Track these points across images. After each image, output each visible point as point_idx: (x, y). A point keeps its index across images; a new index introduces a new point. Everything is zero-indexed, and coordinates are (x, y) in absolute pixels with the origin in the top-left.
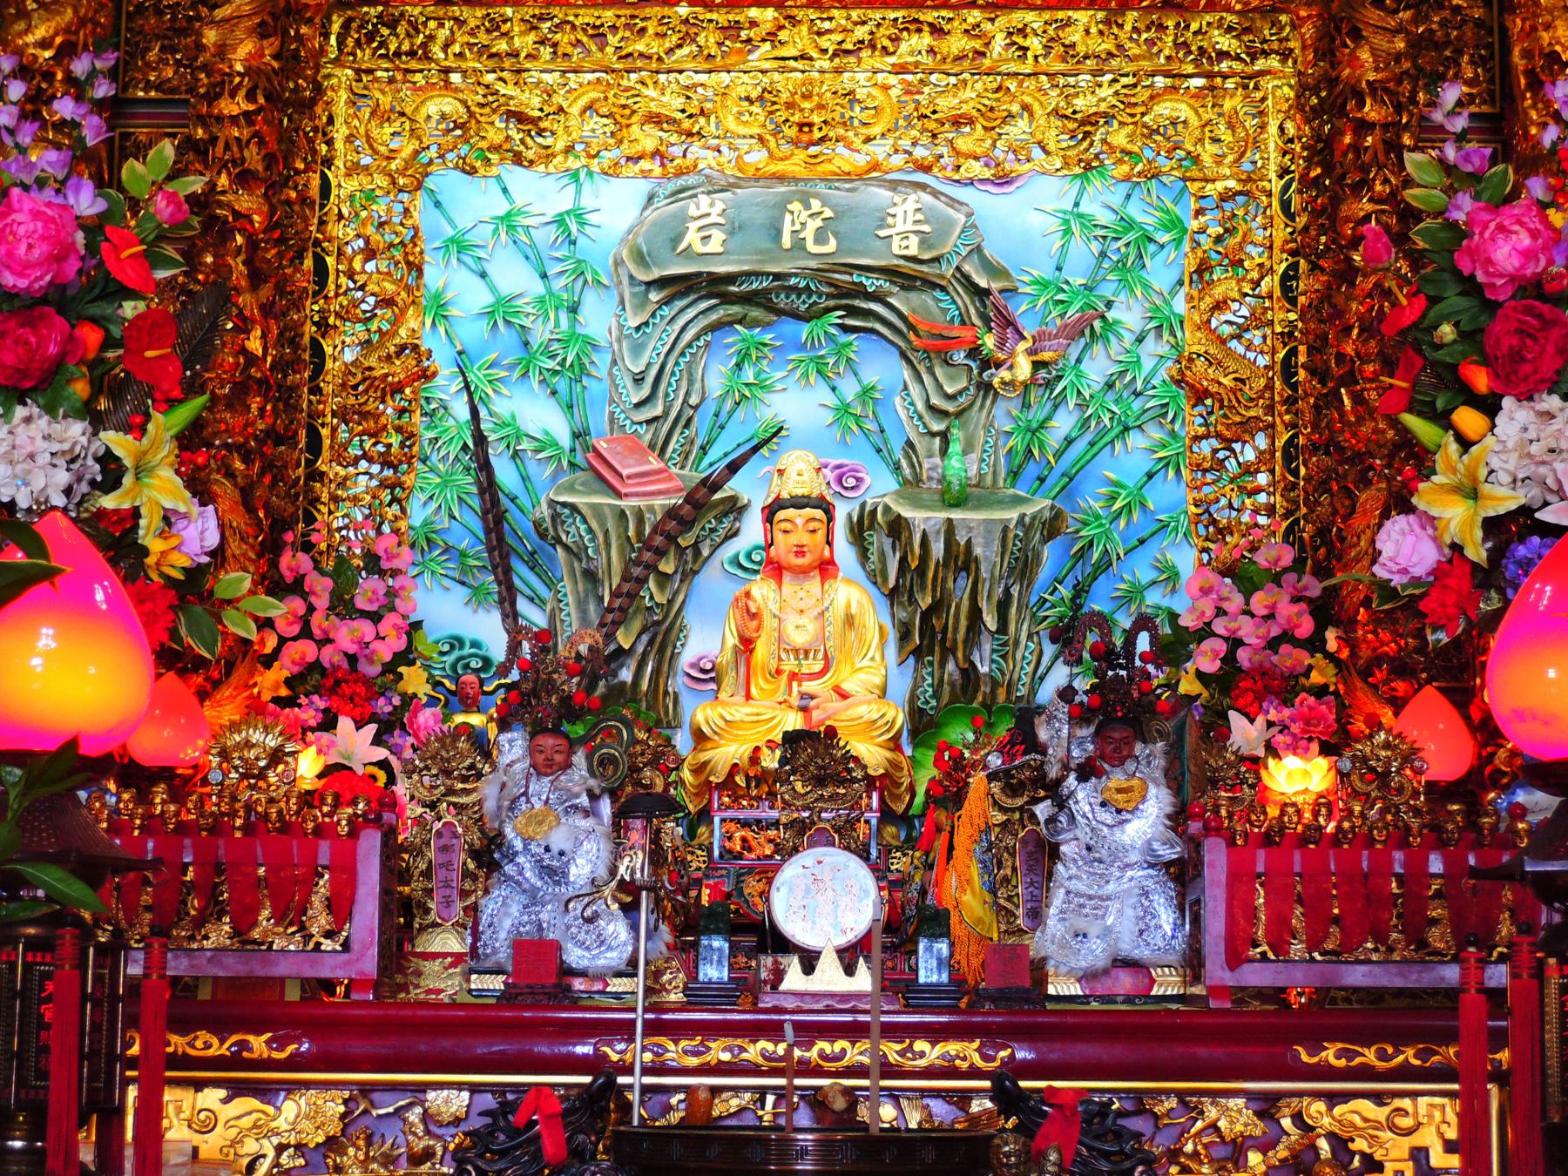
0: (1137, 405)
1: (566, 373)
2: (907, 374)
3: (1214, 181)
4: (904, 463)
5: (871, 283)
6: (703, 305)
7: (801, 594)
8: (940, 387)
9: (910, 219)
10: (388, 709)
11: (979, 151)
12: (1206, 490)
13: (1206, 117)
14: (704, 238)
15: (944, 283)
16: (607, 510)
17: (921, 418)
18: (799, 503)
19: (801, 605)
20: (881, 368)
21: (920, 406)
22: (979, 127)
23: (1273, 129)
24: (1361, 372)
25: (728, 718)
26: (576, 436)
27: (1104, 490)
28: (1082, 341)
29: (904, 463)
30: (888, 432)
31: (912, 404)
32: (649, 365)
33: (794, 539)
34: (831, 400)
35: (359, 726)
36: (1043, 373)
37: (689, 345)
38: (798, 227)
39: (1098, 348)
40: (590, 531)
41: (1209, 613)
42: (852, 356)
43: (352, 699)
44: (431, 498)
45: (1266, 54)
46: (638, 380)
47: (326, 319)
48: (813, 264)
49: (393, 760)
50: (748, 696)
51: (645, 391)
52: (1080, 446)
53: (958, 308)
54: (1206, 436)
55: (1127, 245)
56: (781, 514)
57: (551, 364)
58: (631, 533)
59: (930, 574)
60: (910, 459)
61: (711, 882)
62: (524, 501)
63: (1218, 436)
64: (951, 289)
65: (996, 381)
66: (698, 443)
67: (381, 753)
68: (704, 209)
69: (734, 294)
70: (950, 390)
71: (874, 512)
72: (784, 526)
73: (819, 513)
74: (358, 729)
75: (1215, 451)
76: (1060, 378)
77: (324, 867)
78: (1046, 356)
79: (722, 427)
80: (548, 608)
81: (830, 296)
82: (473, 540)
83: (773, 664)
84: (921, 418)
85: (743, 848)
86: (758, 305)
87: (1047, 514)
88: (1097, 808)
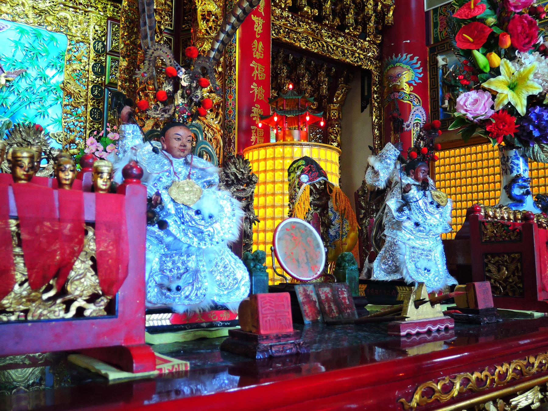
0: (34, 96)
3: (75, 37)
11: (8, 12)
12: (68, 119)
13: (74, 19)
22: (8, 5)
23: (91, 27)
24: (148, 88)
27: (23, 118)
28: (19, 77)
36: (8, 83)
39: (23, 80)
41: (94, 150)
45: (92, 7)
52: (16, 105)
54: (68, 105)
63: (72, 105)
75: (71, 109)
76: (12, 86)
77: (89, 224)
78: (10, 79)
87: (8, 122)
88: (429, 206)
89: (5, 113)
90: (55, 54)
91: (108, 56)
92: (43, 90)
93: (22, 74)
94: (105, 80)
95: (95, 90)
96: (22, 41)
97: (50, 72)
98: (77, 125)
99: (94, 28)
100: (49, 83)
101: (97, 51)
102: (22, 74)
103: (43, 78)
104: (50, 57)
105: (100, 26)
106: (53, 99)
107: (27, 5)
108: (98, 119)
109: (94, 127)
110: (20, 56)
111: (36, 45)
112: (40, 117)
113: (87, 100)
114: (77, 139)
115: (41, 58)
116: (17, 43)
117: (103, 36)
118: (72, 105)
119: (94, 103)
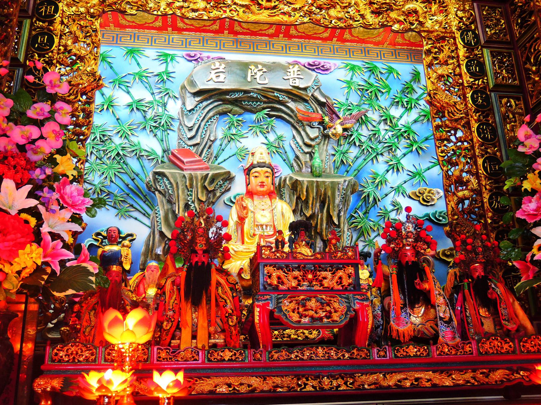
1: (159, 126)
2: (294, 132)
4: (295, 165)
5: (282, 97)
6: (216, 104)
7: (263, 203)
8: (308, 135)
9: (296, 73)
10: (42, 177)
14: (217, 77)
15: (308, 99)
16: (177, 175)
17: (300, 147)
18: (261, 165)
19: (263, 208)
20: (284, 130)
21: (301, 143)
25: (236, 249)
26: (164, 151)
27: (371, 176)
29: (295, 165)
30: (288, 153)
31: (297, 143)
32: (194, 124)
33: (259, 180)
34: (265, 141)
35: (18, 186)
37: (210, 118)
38: (253, 74)
39: (364, 127)
40: (170, 183)
42: (273, 125)
43: (15, 167)
44: (103, 174)
46: (190, 129)
47: (52, 60)
48: (259, 87)
49: (42, 209)
50: (243, 243)
51: (193, 133)
52: (360, 160)
53: (313, 109)
55: (371, 92)
56: (254, 170)
57: (154, 124)
58: (188, 184)
59: (310, 202)
60: (297, 163)
61: (260, 303)
62: (142, 176)
64: (310, 102)
65: (330, 133)
66: (214, 155)
67: (33, 202)
68: (217, 66)
69: (228, 99)
70: (312, 136)
71: (285, 180)
72: (257, 174)
73: (269, 170)
74: (17, 189)
78: (348, 126)
79: (223, 150)
80: (151, 218)
81: (265, 102)
82: (120, 190)
83: (252, 232)
84: (300, 147)
85: (278, 282)
86: (237, 106)
89: (348, 172)
90: (399, 88)
91: (485, 50)
92: (390, 136)
93: (362, 120)
94: (488, 83)
95: (477, 98)
96: (354, 79)
97: (396, 112)
98: (461, 154)
99: (457, 15)
100: (396, 125)
101: (467, 45)
102: (362, 120)
103: (387, 120)
104: (392, 93)
105: (464, 10)
106: (406, 146)
107: (361, 5)
108: (492, 140)
109: (487, 153)
110: (354, 99)
111: (372, 81)
112: (393, 172)
113: (467, 114)
114: (464, 174)
115: (381, 96)
116: (349, 83)
117: (471, 23)
118: (447, 126)
119: (479, 116)
